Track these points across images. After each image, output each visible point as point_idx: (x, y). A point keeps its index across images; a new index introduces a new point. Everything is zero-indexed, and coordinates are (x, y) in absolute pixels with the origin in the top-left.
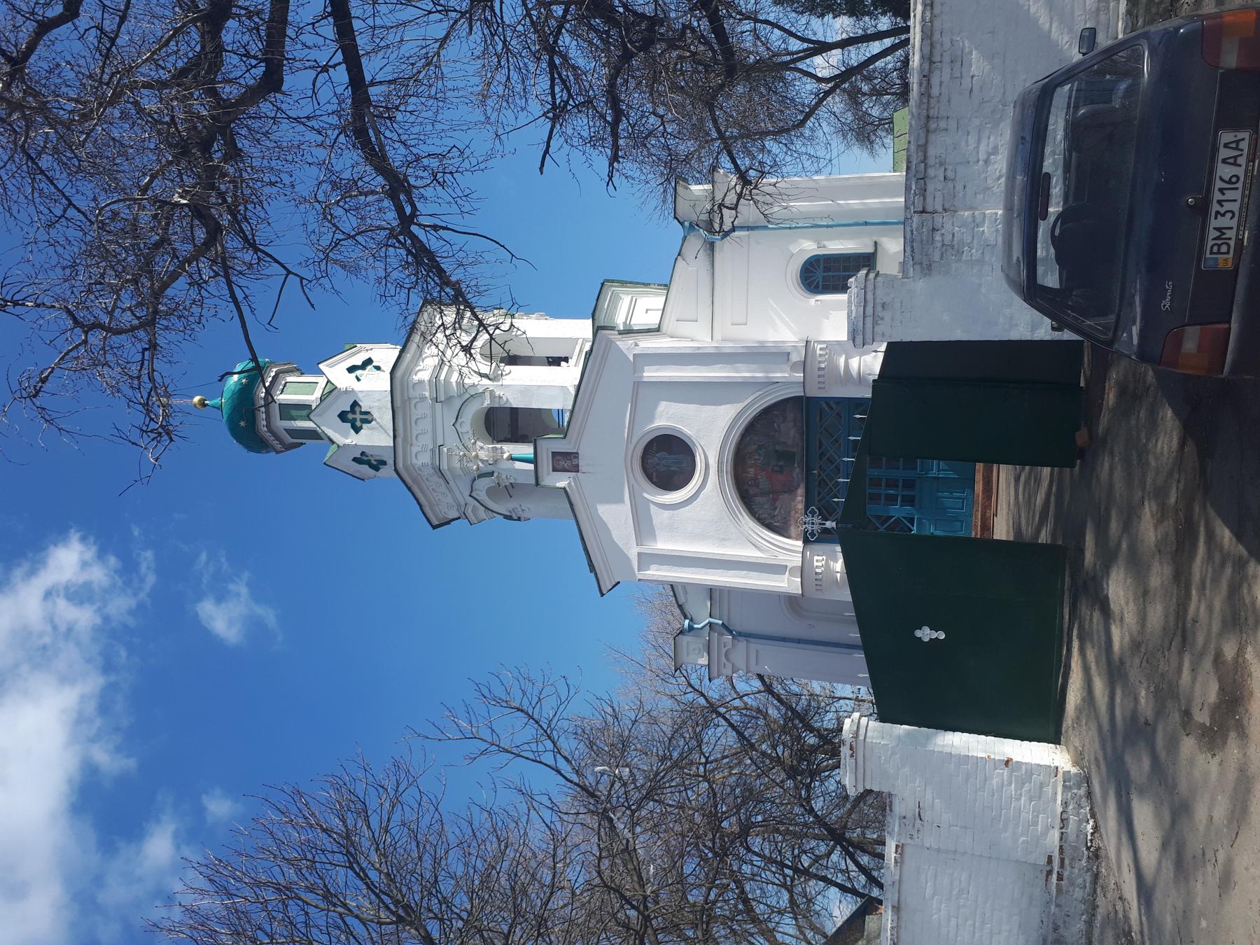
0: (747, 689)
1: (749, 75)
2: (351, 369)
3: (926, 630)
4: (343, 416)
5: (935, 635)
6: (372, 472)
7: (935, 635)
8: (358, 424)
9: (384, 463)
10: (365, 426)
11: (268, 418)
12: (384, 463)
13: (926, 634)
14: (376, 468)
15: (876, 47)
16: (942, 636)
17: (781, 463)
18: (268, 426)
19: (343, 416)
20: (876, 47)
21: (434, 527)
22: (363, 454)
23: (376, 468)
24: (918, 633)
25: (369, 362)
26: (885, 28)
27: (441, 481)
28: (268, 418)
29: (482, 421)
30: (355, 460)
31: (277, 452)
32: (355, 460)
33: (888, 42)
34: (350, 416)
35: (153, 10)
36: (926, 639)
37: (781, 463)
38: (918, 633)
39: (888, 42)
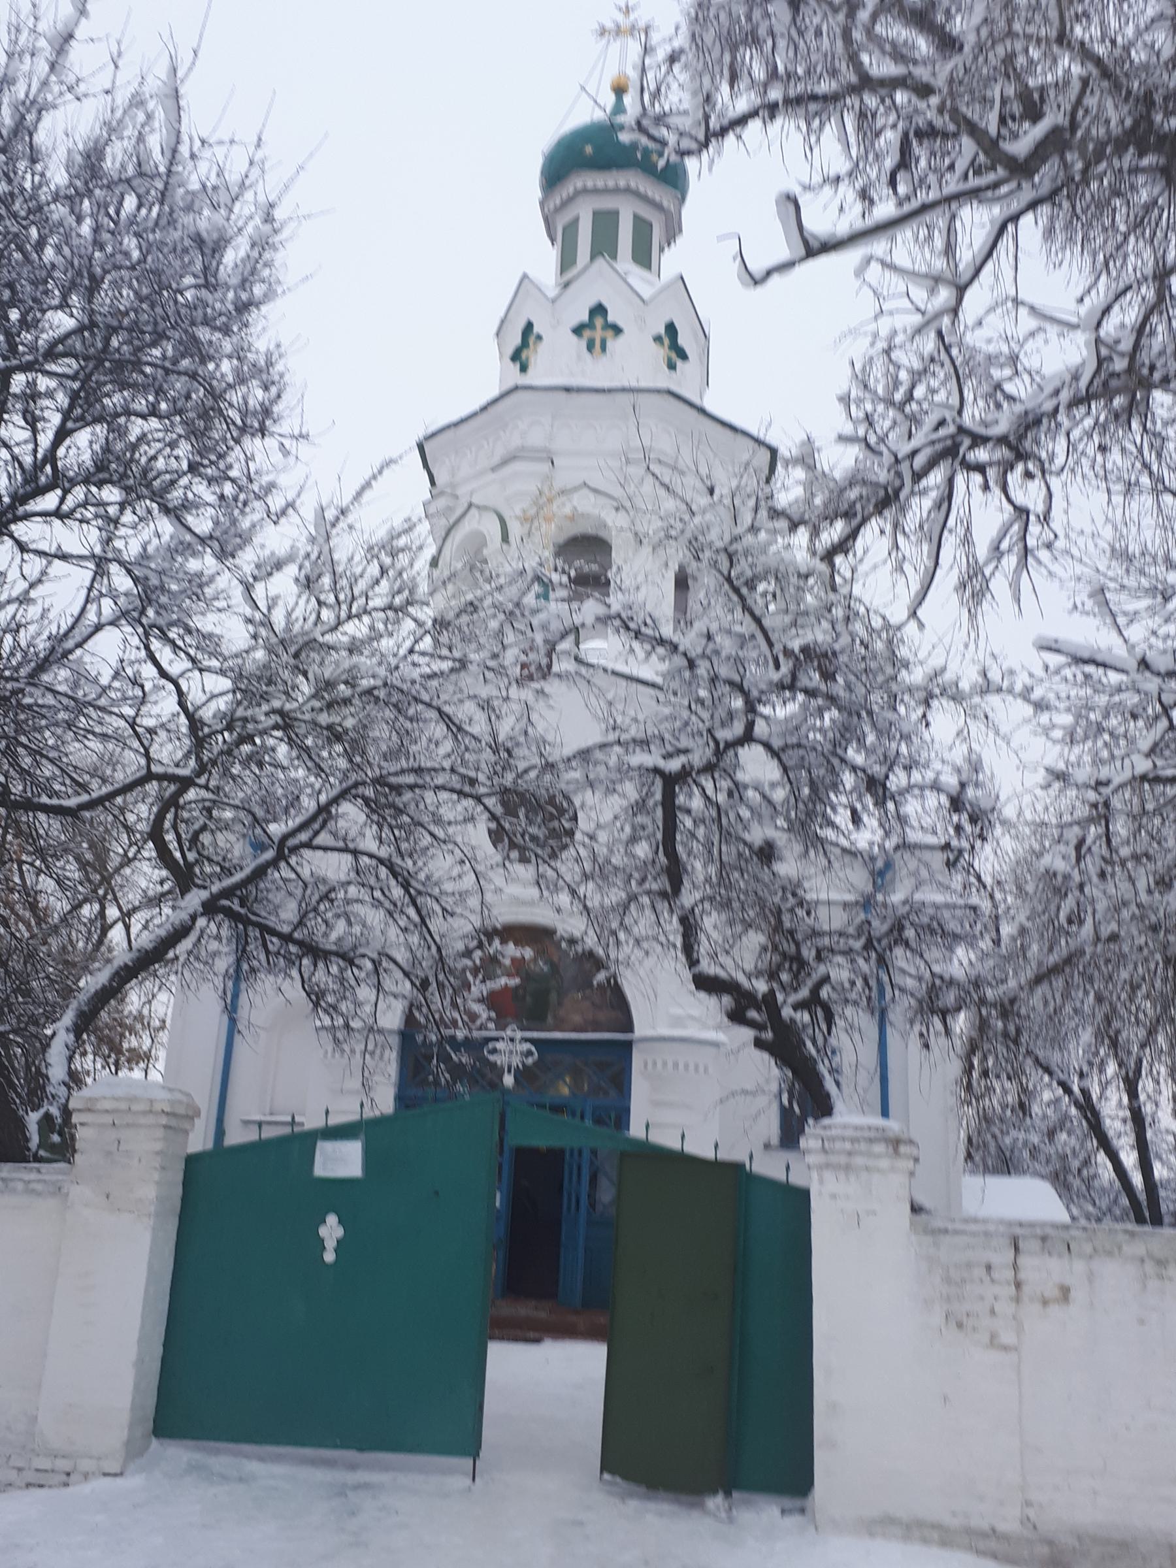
2: (671, 329)
4: (599, 310)
5: (330, 1244)
6: (510, 350)
7: (330, 1244)
8: (587, 333)
9: (524, 369)
10: (583, 344)
11: (596, 191)
12: (524, 369)
13: (331, 1230)
14: (516, 356)
15: (1129, 1159)
16: (329, 1257)
17: (528, 999)
18: (585, 191)
19: (599, 310)
20: (1129, 1159)
21: (421, 447)
23: (516, 356)
24: (332, 1219)
25: (683, 355)
27: (496, 460)
28: (596, 191)
29: (591, 531)
30: (529, 326)
32: (529, 326)
33: (1137, 1179)
34: (599, 322)
35: (1170, 772)
36: (323, 1231)
37: (528, 999)
38: (332, 1219)
39: (1137, 1179)
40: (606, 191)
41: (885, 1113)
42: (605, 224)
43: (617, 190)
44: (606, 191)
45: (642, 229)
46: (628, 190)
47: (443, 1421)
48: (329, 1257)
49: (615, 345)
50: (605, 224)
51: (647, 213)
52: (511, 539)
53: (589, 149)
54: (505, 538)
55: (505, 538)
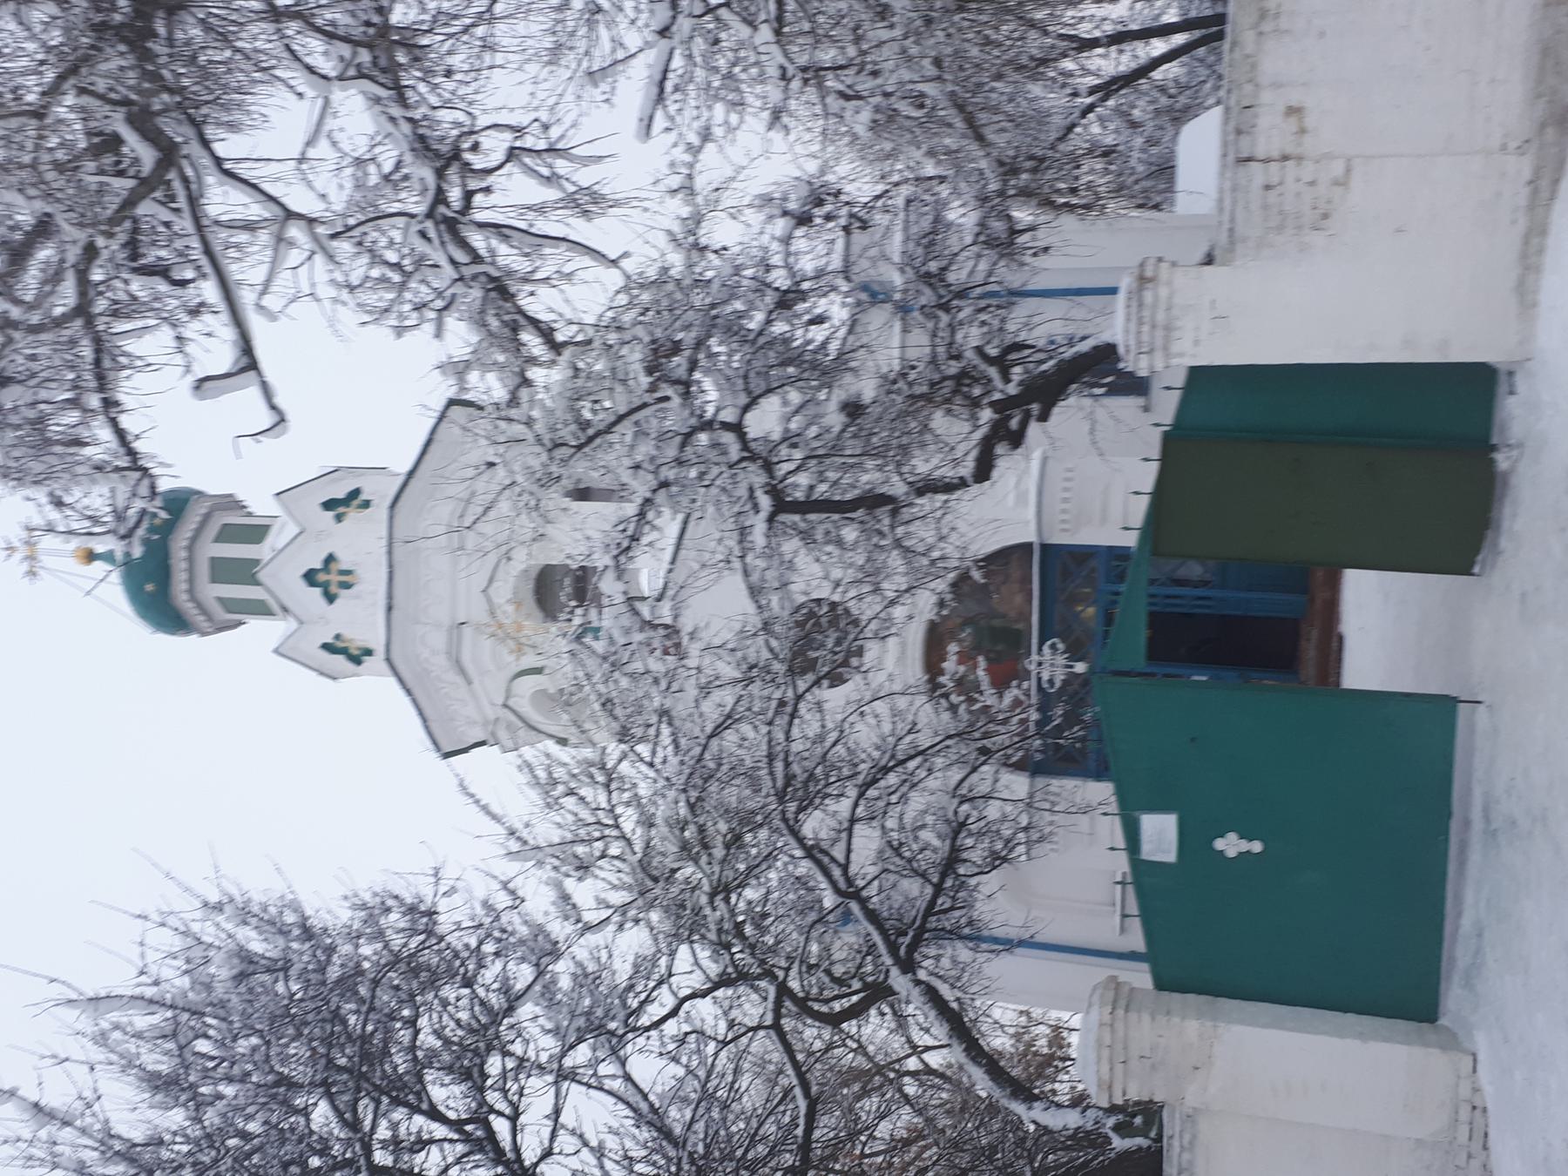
0: (928, 1040)
1: (1150, 280)
2: (329, 505)
3: (1232, 836)
4: (310, 577)
5: (1244, 846)
6: (350, 666)
7: (1244, 846)
8: (333, 589)
9: (369, 652)
10: (344, 593)
13: (1230, 845)
14: (357, 660)
15: (1159, 47)
16: (1257, 847)
17: (999, 647)
19: (310, 577)
20: (1159, 47)
21: (447, 755)
22: (338, 637)
24: (1219, 844)
25: (355, 493)
26: (1174, 20)
27: (460, 680)
29: (531, 585)
30: (326, 647)
31: (204, 634)
32: (326, 647)
33: (1179, 39)
34: (322, 577)
36: (1231, 853)
37: (999, 647)
38: (1219, 844)
39: (1179, 39)
40: (191, 570)
43: (191, 560)
44: (191, 570)
45: (230, 534)
47: (1422, 730)
48: (1257, 847)
49: (345, 561)
50: (225, 571)
53: (149, 587)
54: (538, 671)
55: (538, 671)
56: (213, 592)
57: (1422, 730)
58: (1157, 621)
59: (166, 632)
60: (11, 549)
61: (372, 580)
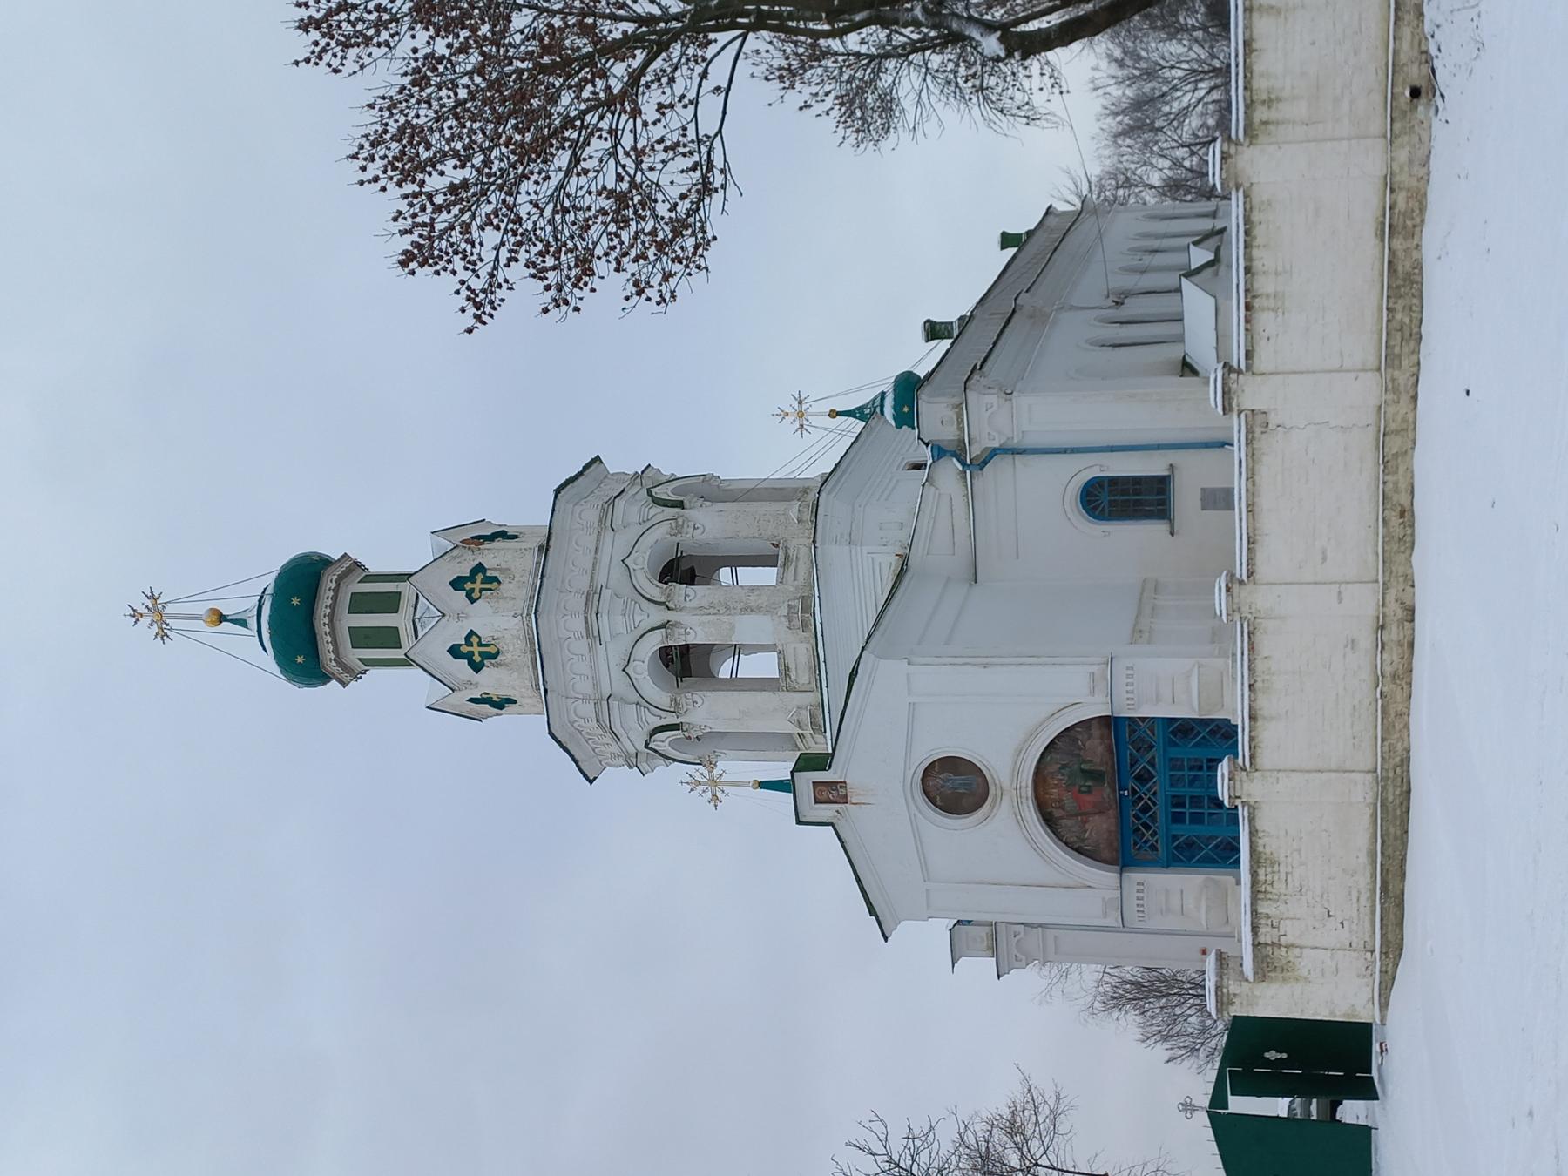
2: (457, 584)
4: (455, 651)
8: (477, 658)
11: (336, 651)
16: (1284, 1056)
24: (1267, 1055)
25: (480, 568)
28: (336, 651)
34: (465, 649)
38: (1267, 1055)
40: (335, 643)
41: (1224, 444)
42: (362, 638)
43: (333, 633)
44: (335, 643)
45: (361, 604)
46: (331, 624)
47: (1363, 1134)
48: (1284, 1056)
49: (485, 634)
50: (362, 638)
51: (345, 602)
52: (677, 721)
53: (300, 660)
54: (676, 727)
55: (676, 727)
56: (353, 656)
57: (1363, 1134)
58: (1230, 507)
59: (308, 685)
60: (136, 615)
61: (514, 650)
